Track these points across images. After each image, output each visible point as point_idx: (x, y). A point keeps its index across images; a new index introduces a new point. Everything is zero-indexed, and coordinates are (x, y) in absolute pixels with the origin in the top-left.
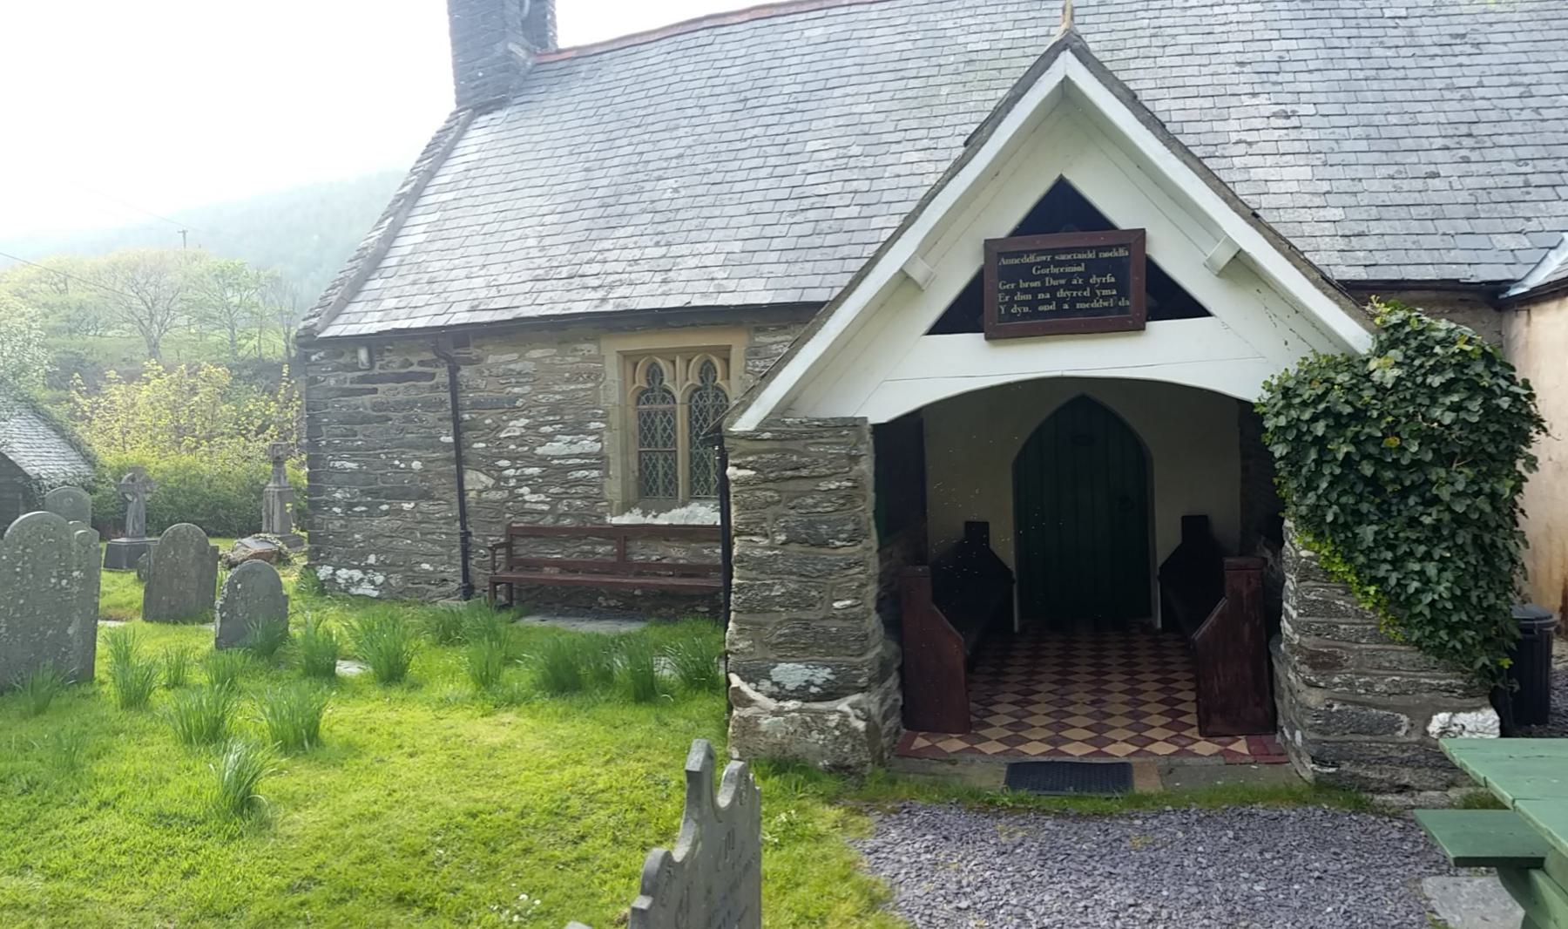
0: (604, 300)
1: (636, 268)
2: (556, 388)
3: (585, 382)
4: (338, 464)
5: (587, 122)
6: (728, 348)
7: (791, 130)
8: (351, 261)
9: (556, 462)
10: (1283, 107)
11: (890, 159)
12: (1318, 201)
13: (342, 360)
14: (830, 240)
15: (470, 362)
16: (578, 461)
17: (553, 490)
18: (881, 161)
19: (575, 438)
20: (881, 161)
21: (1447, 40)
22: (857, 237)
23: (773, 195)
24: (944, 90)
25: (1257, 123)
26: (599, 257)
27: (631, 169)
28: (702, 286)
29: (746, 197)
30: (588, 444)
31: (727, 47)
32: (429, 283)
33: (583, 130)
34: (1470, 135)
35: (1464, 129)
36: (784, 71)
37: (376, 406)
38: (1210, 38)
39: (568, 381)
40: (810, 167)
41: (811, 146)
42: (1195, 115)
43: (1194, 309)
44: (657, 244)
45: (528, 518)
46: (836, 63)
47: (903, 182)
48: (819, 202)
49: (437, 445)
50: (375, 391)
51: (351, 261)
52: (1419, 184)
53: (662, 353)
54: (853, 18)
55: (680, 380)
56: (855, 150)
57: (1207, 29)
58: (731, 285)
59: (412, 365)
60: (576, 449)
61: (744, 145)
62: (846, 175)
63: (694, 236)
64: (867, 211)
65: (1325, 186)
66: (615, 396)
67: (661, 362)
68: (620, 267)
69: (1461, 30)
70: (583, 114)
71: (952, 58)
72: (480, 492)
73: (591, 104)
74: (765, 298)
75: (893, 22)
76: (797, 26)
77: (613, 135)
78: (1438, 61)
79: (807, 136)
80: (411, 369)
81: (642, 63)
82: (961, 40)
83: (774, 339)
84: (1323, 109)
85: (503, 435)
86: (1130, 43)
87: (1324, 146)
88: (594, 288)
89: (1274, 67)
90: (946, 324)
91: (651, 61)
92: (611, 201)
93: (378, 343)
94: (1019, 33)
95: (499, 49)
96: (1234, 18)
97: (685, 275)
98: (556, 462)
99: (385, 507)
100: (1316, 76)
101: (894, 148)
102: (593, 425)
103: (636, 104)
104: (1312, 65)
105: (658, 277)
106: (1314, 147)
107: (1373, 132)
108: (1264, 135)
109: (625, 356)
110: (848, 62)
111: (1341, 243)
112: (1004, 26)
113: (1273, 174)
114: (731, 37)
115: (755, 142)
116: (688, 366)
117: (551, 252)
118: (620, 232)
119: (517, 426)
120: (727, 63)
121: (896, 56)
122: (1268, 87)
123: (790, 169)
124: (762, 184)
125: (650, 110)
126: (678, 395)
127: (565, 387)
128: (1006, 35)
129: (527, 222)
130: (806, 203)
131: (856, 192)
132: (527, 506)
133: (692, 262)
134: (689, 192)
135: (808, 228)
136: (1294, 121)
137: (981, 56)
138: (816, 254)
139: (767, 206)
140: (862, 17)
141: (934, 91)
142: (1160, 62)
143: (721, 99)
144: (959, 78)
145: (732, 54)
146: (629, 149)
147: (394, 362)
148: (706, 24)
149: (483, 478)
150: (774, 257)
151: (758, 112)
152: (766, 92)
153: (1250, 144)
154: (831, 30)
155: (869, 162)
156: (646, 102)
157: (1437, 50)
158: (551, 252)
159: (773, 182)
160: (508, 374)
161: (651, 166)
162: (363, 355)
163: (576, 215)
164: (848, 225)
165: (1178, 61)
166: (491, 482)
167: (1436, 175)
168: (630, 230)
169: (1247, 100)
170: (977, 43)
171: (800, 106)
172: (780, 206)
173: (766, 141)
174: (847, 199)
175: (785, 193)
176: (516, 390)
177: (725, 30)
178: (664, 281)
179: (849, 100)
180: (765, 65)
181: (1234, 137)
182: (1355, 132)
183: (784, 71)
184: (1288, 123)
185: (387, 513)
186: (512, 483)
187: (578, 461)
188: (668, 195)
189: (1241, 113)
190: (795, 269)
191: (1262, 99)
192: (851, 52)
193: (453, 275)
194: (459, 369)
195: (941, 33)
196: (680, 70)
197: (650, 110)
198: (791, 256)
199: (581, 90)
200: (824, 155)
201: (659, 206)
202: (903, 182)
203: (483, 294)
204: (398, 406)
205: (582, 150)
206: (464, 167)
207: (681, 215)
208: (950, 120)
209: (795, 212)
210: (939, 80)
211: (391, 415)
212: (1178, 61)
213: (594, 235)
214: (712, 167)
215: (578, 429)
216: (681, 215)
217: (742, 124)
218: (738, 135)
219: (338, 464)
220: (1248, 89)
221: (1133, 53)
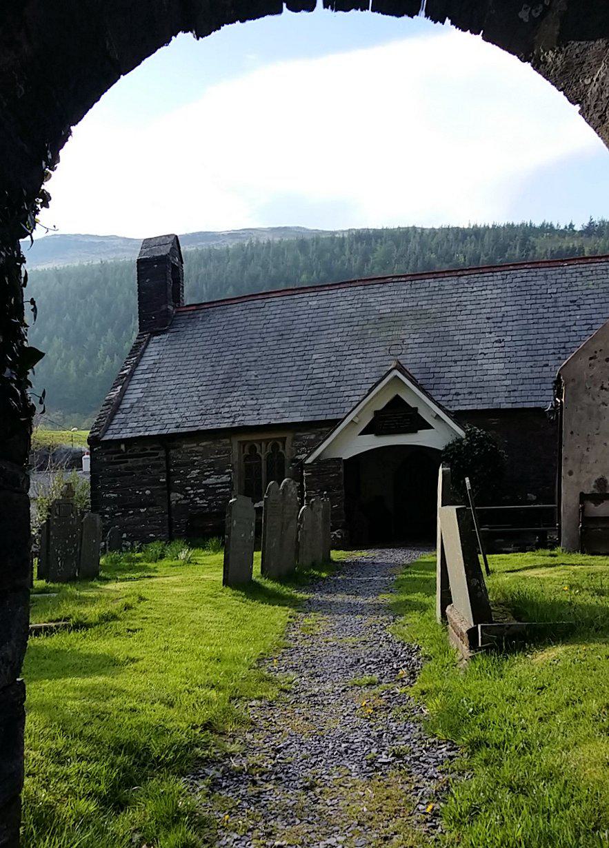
0: (233, 422)
1: (244, 409)
2: (212, 457)
3: (224, 454)
4: (107, 495)
5: (207, 343)
6: (285, 438)
7: (306, 349)
8: (104, 406)
9: (211, 486)
10: (500, 338)
11: (347, 362)
12: (503, 377)
13: (110, 450)
14: (325, 396)
15: (174, 448)
16: (220, 485)
17: (209, 498)
18: (343, 363)
19: (219, 476)
20: (343, 363)
21: (569, 303)
22: (335, 395)
23: (299, 378)
24: (370, 332)
25: (489, 345)
26: (227, 405)
27: (234, 366)
28: (274, 416)
29: (288, 379)
30: (225, 478)
31: (272, 309)
32: (152, 415)
33: (206, 347)
34: (564, 348)
35: (562, 345)
36: (300, 321)
37: (126, 468)
38: (478, 306)
39: (217, 454)
40: (314, 366)
41: (315, 357)
42: (468, 342)
43: (429, 427)
44: (252, 399)
45: (198, 510)
46: (324, 318)
47: (352, 372)
48: (320, 381)
49: (157, 482)
50: (127, 462)
51: (104, 406)
52: (540, 369)
53: (257, 441)
54: (330, 297)
55: (263, 452)
56: (333, 359)
57: (478, 302)
58: (287, 415)
59: (147, 450)
60: (219, 481)
61: (284, 356)
62: (330, 369)
63: (267, 396)
64: (338, 384)
65: (507, 371)
66: (236, 459)
67: (257, 445)
68: (238, 409)
69: (575, 298)
70: (205, 339)
71: (373, 317)
72: (177, 501)
73: (207, 334)
74: (301, 419)
75: (347, 299)
76: (305, 300)
77: (221, 350)
78: (563, 314)
79: (312, 352)
80: (147, 452)
81: (230, 315)
82: (377, 308)
83: (301, 434)
84: (514, 338)
85: (188, 477)
86: (448, 309)
87: (510, 354)
88: (228, 418)
89: (500, 320)
90: (364, 432)
91: (235, 314)
92: (227, 380)
93: (128, 442)
94: (406, 305)
95: (164, 307)
96: (489, 297)
97: (266, 412)
98: (211, 486)
99: (131, 512)
100: (515, 323)
101: (348, 357)
102: (227, 471)
103: (231, 335)
104: (515, 318)
105: (256, 413)
106: (508, 355)
107: (530, 347)
108: (490, 350)
109: (243, 444)
110: (329, 318)
111: (507, 394)
112: (398, 301)
113: (490, 367)
114: (272, 304)
115: (290, 355)
116: (266, 446)
117: (205, 402)
118: (235, 394)
119: (195, 473)
120: (273, 317)
121: (348, 315)
122: (496, 329)
123: (307, 367)
124: (295, 373)
125: (239, 338)
126: (263, 457)
127: (216, 456)
128: (400, 305)
129: (191, 390)
130: (314, 381)
131: (334, 376)
132: (199, 505)
133: (268, 406)
134: (262, 377)
135: (315, 392)
136: (503, 344)
137: (387, 315)
138: (318, 402)
139: (298, 383)
140: (334, 296)
141: (365, 332)
142: (459, 318)
143: (272, 334)
144: (376, 326)
145: (274, 312)
146: (232, 357)
147: (137, 449)
148: (260, 297)
149: (179, 495)
150: (303, 403)
151: (290, 341)
152: (293, 332)
153: (485, 354)
154: (320, 302)
155: (339, 363)
156: (236, 334)
157: (563, 309)
158: (205, 402)
159: (300, 372)
160: (191, 452)
161: (243, 365)
162: (123, 447)
163: (212, 387)
164: (331, 390)
165: (465, 317)
166: (182, 496)
167: (547, 365)
168: (239, 393)
169: (488, 335)
170: (385, 309)
171: (309, 338)
172: (303, 382)
173: (294, 354)
174: (331, 379)
175: (305, 377)
176: (195, 458)
177: (269, 300)
178: (258, 414)
179: (330, 336)
180: (291, 318)
181: (480, 351)
182: (523, 348)
183: (300, 321)
184: (500, 345)
185: (132, 514)
186: (192, 496)
187: (220, 485)
188: (253, 378)
189: (485, 341)
190: (311, 408)
191: (493, 335)
192: (330, 313)
193: (162, 412)
194: (169, 451)
195: (368, 304)
196: (249, 319)
197: (239, 338)
198: (309, 403)
199: (201, 327)
200: (321, 361)
201: (250, 383)
202: (352, 372)
203: (180, 420)
204: (139, 468)
205: (208, 357)
206: (152, 362)
207: (260, 387)
208: (372, 345)
209: (309, 385)
210: (368, 327)
211: (135, 472)
212: (465, 317)
213: (222, 396)
214: (271, 366)
215: (221, 472)
216: (260, 387)
217: (282, 347)
218: (281, 351)
219: (107, 495)
220: (489, 330)
221: (449, 314)
